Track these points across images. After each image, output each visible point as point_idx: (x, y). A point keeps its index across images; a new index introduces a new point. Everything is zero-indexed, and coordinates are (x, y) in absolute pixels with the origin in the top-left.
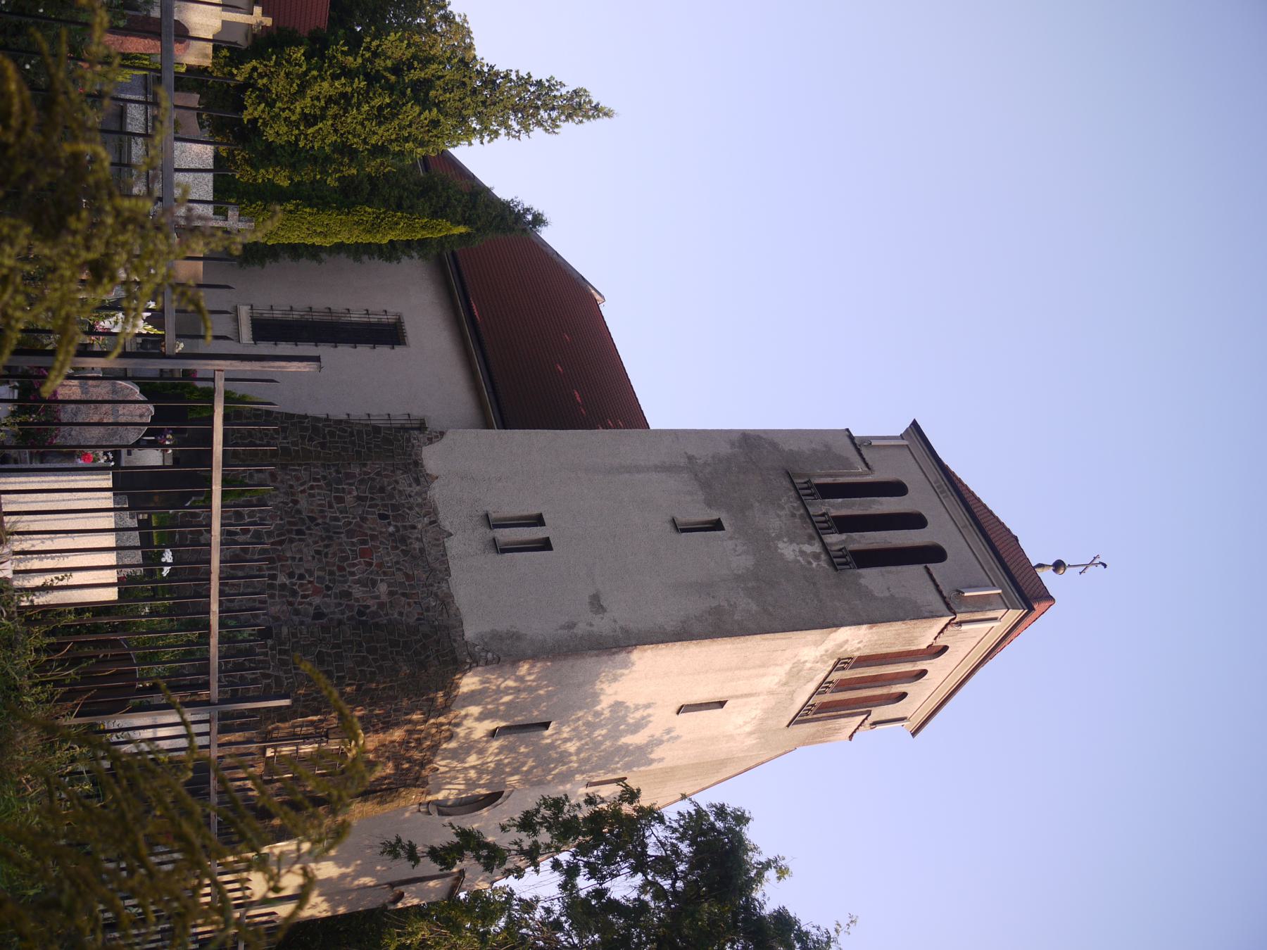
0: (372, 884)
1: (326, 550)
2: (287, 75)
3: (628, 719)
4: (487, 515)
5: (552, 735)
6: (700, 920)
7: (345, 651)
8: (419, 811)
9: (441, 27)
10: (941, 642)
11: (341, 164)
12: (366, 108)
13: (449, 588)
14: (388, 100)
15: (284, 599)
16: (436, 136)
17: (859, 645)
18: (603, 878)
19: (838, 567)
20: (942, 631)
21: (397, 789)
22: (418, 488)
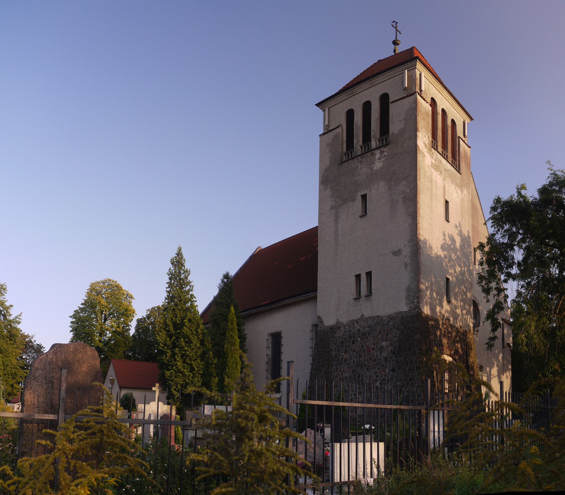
0: (502, 355)
2: (176, 377)
3: (449, 244)
5: (452, 277)
6: (536, 225)
7: (409, 360)
8: (476, 334)
9: (152, 319)
10: (429, 100)
11: (208, 357)
12: (186, 348)
14: (182, 340)
16: (195, 320)
17: (427, 137)
18: (513, 262)
19: (388, 143)
20: (424, 99)
21: (467, 343)
22: (342, 328)
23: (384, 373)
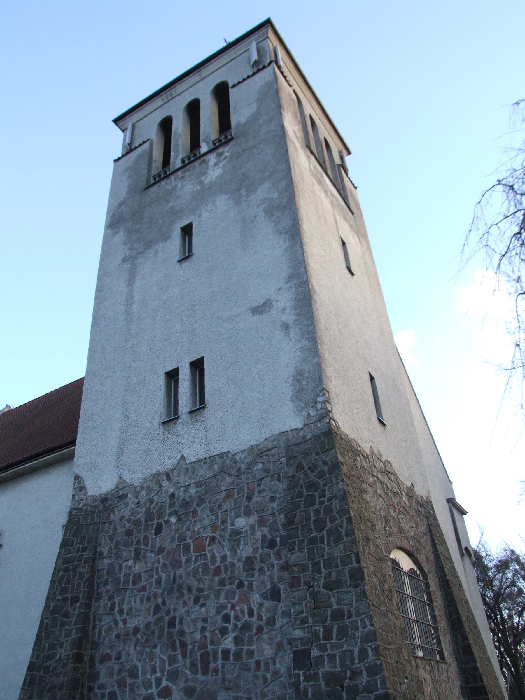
1: (194, 591)
4: (164, 423)
7: (323, 556)
13: (242, 452)
15: (255, 638)
22: (129, 496)
23: (245, 606)
